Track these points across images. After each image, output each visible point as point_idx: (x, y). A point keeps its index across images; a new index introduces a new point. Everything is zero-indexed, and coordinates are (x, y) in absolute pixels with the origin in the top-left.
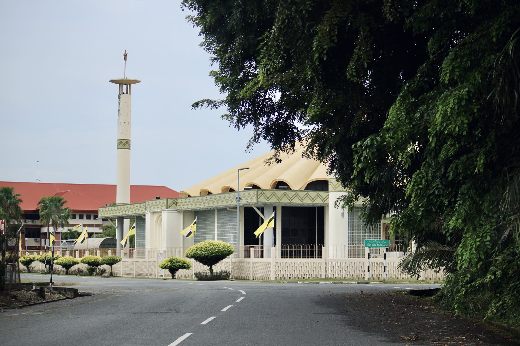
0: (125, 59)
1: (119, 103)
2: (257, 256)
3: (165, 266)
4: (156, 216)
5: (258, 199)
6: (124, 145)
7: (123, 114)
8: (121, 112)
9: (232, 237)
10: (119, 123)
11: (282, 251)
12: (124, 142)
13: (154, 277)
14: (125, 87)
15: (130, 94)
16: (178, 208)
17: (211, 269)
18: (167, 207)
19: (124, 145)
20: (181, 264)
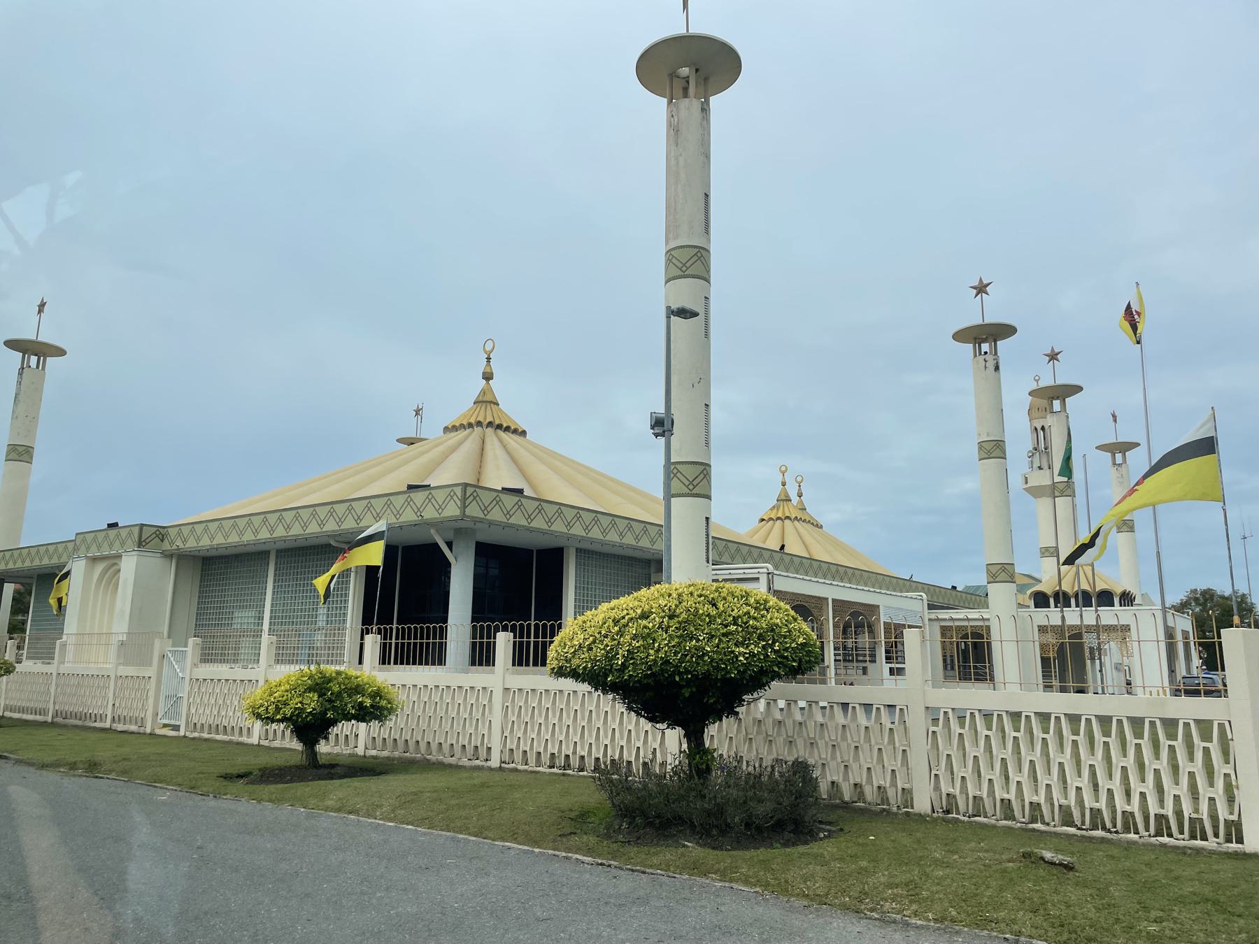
0: (40, 311)
1: (19, 383)
2: (521, 658)
4: (100, 567)
6: (20, 454)
7: (27, 396)
8: (21, 397)
10: (15, 416)
11: (474, 644)
12: (20, 449)
13: (133, 728)
16: (166, 546)
18: (140, 543)
20: (368, 702)
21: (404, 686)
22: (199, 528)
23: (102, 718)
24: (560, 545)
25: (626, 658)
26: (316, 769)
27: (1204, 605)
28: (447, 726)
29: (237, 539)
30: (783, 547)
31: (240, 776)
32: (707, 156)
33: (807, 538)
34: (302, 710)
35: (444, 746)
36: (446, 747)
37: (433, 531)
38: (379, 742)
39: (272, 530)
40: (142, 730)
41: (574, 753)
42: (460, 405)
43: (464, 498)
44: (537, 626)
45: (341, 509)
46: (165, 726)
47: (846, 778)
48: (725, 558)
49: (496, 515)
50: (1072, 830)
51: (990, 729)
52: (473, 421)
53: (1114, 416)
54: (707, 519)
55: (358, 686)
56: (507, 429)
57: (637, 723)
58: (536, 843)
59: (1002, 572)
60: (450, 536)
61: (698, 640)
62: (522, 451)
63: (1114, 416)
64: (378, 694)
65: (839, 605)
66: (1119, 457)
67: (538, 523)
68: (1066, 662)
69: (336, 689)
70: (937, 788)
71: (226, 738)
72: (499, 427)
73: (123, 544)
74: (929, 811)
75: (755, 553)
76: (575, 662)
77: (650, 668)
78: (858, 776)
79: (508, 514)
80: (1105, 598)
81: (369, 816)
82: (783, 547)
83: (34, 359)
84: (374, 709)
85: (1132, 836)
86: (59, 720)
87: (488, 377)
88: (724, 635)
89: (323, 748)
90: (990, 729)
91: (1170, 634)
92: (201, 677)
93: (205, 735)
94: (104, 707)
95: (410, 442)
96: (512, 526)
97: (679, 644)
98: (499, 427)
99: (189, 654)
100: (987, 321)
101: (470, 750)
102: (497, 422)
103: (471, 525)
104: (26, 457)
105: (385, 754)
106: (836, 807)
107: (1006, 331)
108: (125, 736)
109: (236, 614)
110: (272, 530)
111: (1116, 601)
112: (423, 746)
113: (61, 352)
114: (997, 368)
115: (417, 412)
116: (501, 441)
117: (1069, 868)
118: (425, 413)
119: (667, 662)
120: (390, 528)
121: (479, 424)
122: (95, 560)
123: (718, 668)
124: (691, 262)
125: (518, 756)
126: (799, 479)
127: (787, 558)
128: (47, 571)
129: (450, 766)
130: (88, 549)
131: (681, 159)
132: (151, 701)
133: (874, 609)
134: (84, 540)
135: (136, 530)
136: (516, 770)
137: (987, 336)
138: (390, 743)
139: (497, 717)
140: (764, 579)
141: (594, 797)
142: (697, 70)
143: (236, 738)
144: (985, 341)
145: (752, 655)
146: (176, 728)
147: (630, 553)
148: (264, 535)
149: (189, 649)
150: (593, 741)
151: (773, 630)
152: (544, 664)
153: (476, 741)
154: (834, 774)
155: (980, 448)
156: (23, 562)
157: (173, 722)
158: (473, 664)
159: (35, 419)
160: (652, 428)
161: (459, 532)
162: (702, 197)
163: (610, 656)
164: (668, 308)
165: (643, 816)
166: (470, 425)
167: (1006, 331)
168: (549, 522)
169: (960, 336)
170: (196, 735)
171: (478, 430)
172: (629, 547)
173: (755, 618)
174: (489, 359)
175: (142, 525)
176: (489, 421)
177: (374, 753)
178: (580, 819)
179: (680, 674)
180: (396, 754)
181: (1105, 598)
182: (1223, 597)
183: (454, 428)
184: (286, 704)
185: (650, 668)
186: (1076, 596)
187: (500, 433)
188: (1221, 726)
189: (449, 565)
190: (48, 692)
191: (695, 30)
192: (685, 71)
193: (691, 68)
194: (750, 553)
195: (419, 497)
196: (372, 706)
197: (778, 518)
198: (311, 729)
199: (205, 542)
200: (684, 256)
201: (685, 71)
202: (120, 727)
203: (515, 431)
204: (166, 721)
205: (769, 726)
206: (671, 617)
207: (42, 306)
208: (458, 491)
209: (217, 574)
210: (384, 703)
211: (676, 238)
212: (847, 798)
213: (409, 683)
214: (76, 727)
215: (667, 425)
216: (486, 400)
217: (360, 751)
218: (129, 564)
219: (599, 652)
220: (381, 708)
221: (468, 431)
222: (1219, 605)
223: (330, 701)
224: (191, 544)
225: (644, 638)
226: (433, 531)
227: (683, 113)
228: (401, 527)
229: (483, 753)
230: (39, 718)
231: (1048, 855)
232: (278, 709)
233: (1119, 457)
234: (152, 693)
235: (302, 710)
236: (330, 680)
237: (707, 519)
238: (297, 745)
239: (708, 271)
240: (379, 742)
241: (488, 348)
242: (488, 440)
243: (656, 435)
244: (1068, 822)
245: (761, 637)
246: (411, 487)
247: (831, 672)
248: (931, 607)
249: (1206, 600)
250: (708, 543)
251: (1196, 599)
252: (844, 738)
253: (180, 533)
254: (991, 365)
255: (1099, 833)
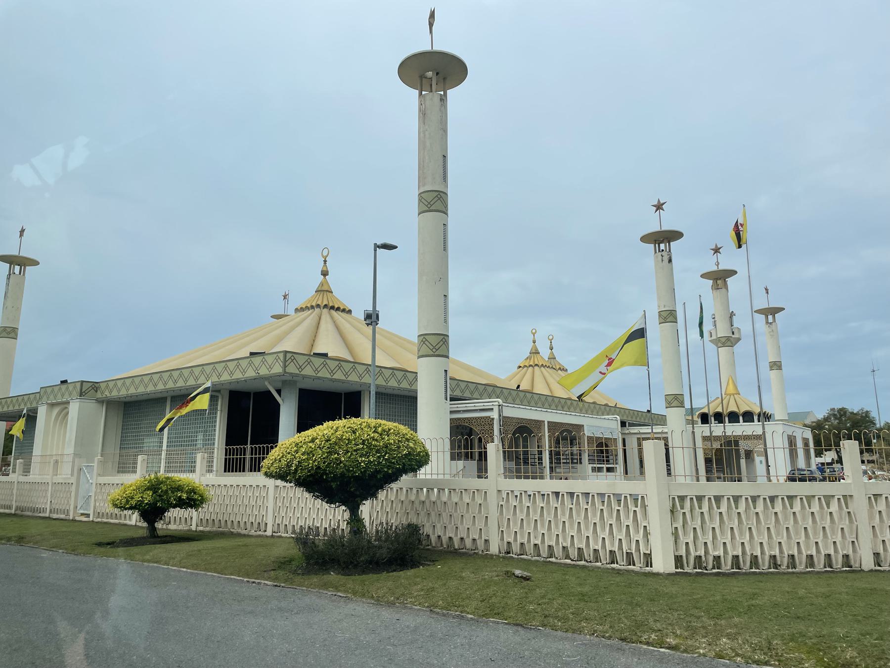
1: (8, 285)
3: (133, 503)
4: (56, 410)
5: (285, 367)
7: (14, 292)
8: (8, 295)
9: (199, 438)
11: (226, 459)
12: (9, 330)
13: (62, 516)
14: (17, 268)
15: (24, 274)
16: (99, 395)
17: (355, 520)
18: (81, 394)
19: (9, 333)
20: (184, 496)
21: (258, 486)
22: (128, 382)
23: (44, 510)
24: (356, 388)
25: (297, 467)
26: (154, 538)
27: (840, 419)
28: (236, 510)
29: (143, 390)
30: (518, 386)
31: (108, 544)
32: (445, 131)
33: (551, 380)
34: (142, 502)
35: (478, 542)
36: (242, 524)
37: (266, 383)
38: (204, 522)
39: (165, 384)
40: (67, 518)
41: (529, 540)
42: (305, 293)
43: (285, 361)
44: (252, 448)
45: (220, 367)
46: (82, 514)
47: (456, 535)
48: (476, 395)
49: (308, 371)
50: (568, 561)
51: (637, 507)
52: (314, 304)
53: (767, 290)
54: (446, 371)
55: (180, 486)
56: (338, 309)
57: (322, 505)
58: (248, 576)
59: (675, 401)
60: (279, 385)
61: (338, 454)
62: (347, 325)
63: (767, 290)
64: (193, 491)
65: (553, 426)
66: (770, 318)
67: (339, 376)
68: (724, 460)
69: (164, 488)
70: (502, 539)
71: (116, 521)
72: (332, 308)
73: (70, 394)
74: (497, 553)
75: (498, 391)
76: (272, 469)
77: (309, 471)
78: (439, 531)
79: (316, 370)
80: (748, 416)
81: (167, 564)
82: (518, 386)
83: (17, 268)
84: (192, 500)
85: (599, 564)
86: (19, 512)
87: (325, 273)
88: (355, 451)
89: (159, 525)
90: (637, 507)
91: (792, 441)
92: (102, 483)
93: (105, 520)
94: (45, 503)
95: (277, 317)
96: (319, 378)
97: (327, 457)
98: (332, 308)
99: (95, 468)
100: (663, 229)
101: (256, 525)
102: (331, 305)
103: (290, 378)
104: (12, 335)
105: (208, 529)
106: (451, 552)
107: (675, 235)
108: (57, 522)
109: (145, 441)
110: (165, 384)
111: (756, 418)
112: (229, 523)
113: (36, 263)
114: (670, 261)
115: (285, 297)
116: (332, 318)
117: (527, 579)
118: (290, 297)
119: (318, 468)
120: (213, 385)
121: (318, 306)
122: (52, 405)
123: (348, 471)
124: (434, 202)
125: (282, 528)
126: (551, 337)
127: (522, 394)
128: (160, 395)
129: (244, 535)
130: (48, 398)
131: (427, 133)
132: (73, 499)
133: (580, 427)
134: (46, 392)
135: (78, 385)
136: (280, 537)
137: (663, 239)
138: (210, 522)
139: (270, 504)
140: (496, 409)
141: (295, 551)
142: (437, 74)
143: (122, 521)
144: (662, 242)
145: (370, 462)
146: (88, 515)
147: (406, 393)
148: (160, 387)
149: (95, 464)
150: (545, 532)
151: (387, 447)
152: (259, 471)
153: (259, 520)
154: (436, 530)
155: (660, 316)
156: (8, 407)
157: (86, 512)
158: (225, 471)
159: (18, 309)
160: (365, 320)
161: (284, 382)
162: (441, 158)
163: (289, 465)
164: (375, 244)
165: (324, 560)
166: (312, 307)
167: (675, 235)
168: (346, 374)
169: (645, 239)
170: (99, 520)
171: (317, 310)
172: (405, 390)
173: (376, 440)
174: (325, 261)
175: (82, 382)
176: (326, 304)
177: (201, 528)
178: (283, 564)
179: (327, 474)
180: (215, 529)
181: (748, 416)
182: (852, 413)
183: (302, 309)
184: (132, 498)
185: (309, 471)
186: (759, 415)
187: (333, 312)
188: (642, 497)
189: (279, 405)
190: (12, 494)
191: (437, 48)
192: (430, 74)
193: (433, 72)
194: (493, 391)
195: (257, 360)
196: (188, 498)
197: (530, 366)
198: (152, 513)
199: (123, 392)
200: (429, 197)
201: (430, 74)
202: (55, 516)
203: (344, 310)
204: (82, 512)
205: (417, 504)
206: (327, 441)
207: (22, 232)
208: (281, 356)
209: (134, 412)
210: (196, 497)
211: (424, 185)
212: (456, 547)
213: (241, 484)
214: (28, 516)
215: (374, 317)
216: (324, 290)
217: (193, 528)
218: (74, 408)
219: (284, 462)
220: (195, 500)
221: (311, 311)
222: (849, 419)
223: (160, 496)
224: (115, 393)
225: (308, 454)
226: (266, 383)
227: (428, 103)
228: (246, 381)
229: (262, 527)
230: (7, 511)
231: (518, 572)
232: (127, 502)
233: (770, 318)
234: (73, 494)
235: (142, 502)
236: (162, 483)
237: (446, 371)
238: (145, 525)
239: (446, 207)
240: (204, 522)
241: (325, 254)
242: (323, 317)
243: (368, 324)
244: (568, 557)
245: (378, 451)
246: (252, 354)
247: (547, 470)
248: (623, 424)
249: (841, 416)
250: (446, 387)
251: (834, 415)
252: (456, 511)
253: (107, 386)
254: (666, 258)
255: (583, 563)
